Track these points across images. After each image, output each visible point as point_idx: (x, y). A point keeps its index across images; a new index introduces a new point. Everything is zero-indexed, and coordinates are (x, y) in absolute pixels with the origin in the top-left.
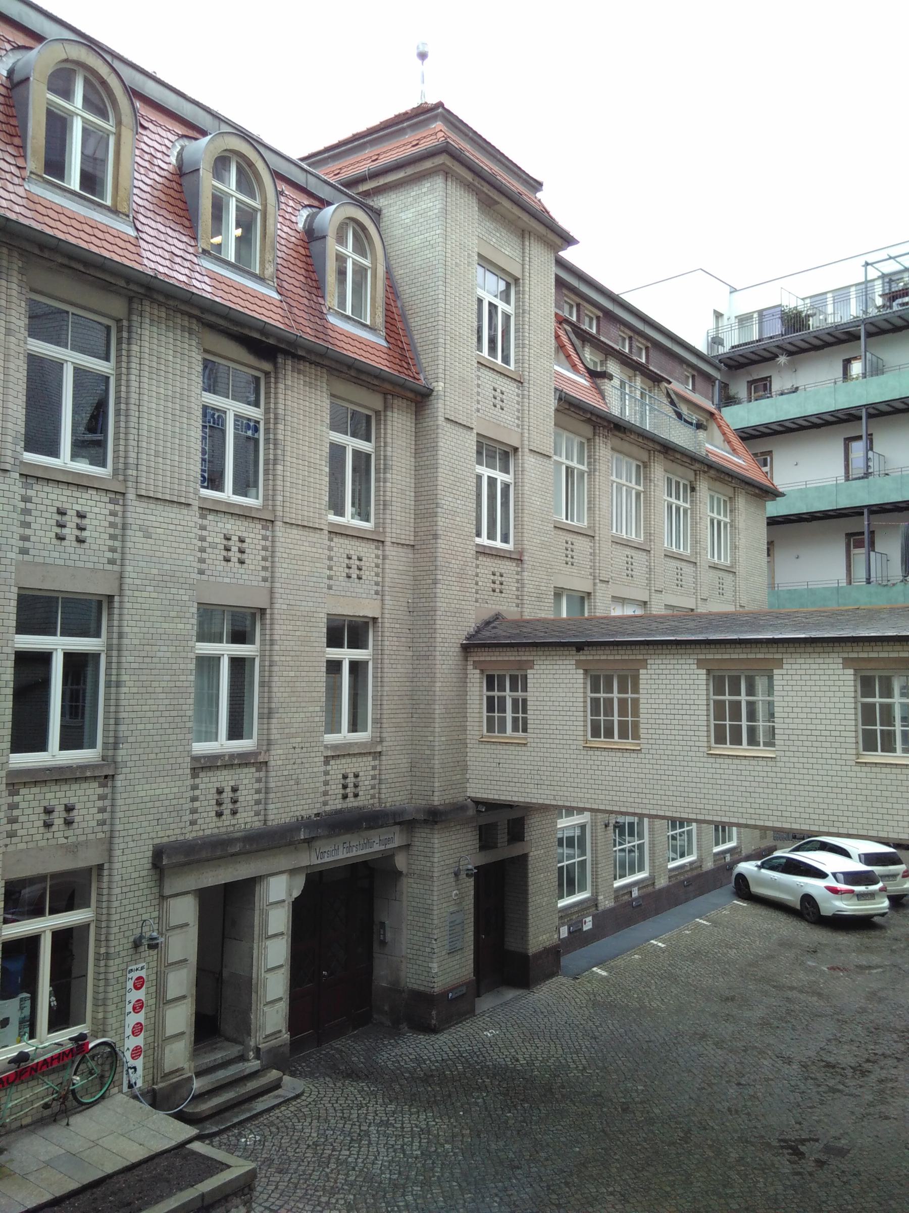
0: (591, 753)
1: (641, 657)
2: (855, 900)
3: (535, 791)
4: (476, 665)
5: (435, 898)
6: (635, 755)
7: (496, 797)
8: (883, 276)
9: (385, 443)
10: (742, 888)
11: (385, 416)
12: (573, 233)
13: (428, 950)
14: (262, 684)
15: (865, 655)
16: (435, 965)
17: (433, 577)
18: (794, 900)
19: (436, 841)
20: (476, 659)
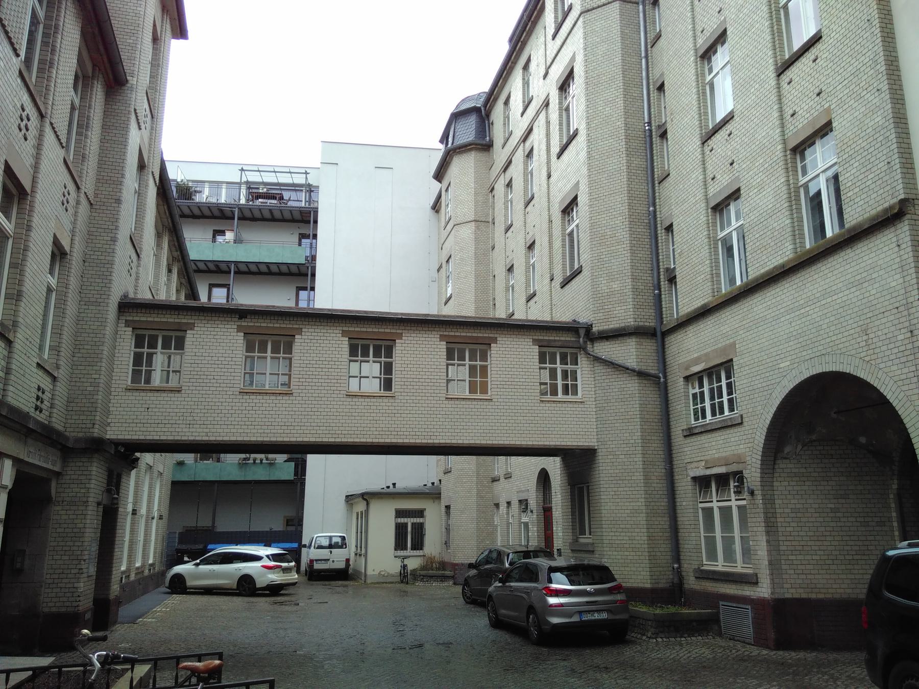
0: (246, 397)
1: (297, 326)
2: (281, 574)
3: (187, 430)
4: (127, 323)
5: (88, 521)
6: (287, 398)
7: (142, 437)
8: (247, 182)
9: (90, 105)
10: (179, 585)
11: (93, 83)
12: (190, 34)
13: (76, 571)
14: (13, 265)
15: (453, 334)
16: (82, 585)
17: (113, 235)
18: (232, 583)
19: (94, 469)
20: (128, 318)
